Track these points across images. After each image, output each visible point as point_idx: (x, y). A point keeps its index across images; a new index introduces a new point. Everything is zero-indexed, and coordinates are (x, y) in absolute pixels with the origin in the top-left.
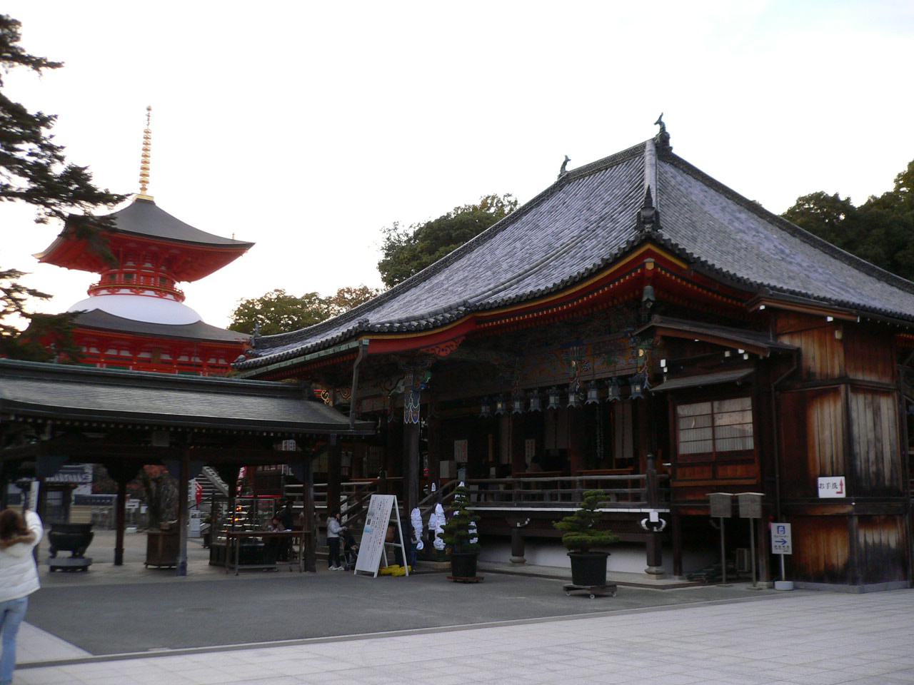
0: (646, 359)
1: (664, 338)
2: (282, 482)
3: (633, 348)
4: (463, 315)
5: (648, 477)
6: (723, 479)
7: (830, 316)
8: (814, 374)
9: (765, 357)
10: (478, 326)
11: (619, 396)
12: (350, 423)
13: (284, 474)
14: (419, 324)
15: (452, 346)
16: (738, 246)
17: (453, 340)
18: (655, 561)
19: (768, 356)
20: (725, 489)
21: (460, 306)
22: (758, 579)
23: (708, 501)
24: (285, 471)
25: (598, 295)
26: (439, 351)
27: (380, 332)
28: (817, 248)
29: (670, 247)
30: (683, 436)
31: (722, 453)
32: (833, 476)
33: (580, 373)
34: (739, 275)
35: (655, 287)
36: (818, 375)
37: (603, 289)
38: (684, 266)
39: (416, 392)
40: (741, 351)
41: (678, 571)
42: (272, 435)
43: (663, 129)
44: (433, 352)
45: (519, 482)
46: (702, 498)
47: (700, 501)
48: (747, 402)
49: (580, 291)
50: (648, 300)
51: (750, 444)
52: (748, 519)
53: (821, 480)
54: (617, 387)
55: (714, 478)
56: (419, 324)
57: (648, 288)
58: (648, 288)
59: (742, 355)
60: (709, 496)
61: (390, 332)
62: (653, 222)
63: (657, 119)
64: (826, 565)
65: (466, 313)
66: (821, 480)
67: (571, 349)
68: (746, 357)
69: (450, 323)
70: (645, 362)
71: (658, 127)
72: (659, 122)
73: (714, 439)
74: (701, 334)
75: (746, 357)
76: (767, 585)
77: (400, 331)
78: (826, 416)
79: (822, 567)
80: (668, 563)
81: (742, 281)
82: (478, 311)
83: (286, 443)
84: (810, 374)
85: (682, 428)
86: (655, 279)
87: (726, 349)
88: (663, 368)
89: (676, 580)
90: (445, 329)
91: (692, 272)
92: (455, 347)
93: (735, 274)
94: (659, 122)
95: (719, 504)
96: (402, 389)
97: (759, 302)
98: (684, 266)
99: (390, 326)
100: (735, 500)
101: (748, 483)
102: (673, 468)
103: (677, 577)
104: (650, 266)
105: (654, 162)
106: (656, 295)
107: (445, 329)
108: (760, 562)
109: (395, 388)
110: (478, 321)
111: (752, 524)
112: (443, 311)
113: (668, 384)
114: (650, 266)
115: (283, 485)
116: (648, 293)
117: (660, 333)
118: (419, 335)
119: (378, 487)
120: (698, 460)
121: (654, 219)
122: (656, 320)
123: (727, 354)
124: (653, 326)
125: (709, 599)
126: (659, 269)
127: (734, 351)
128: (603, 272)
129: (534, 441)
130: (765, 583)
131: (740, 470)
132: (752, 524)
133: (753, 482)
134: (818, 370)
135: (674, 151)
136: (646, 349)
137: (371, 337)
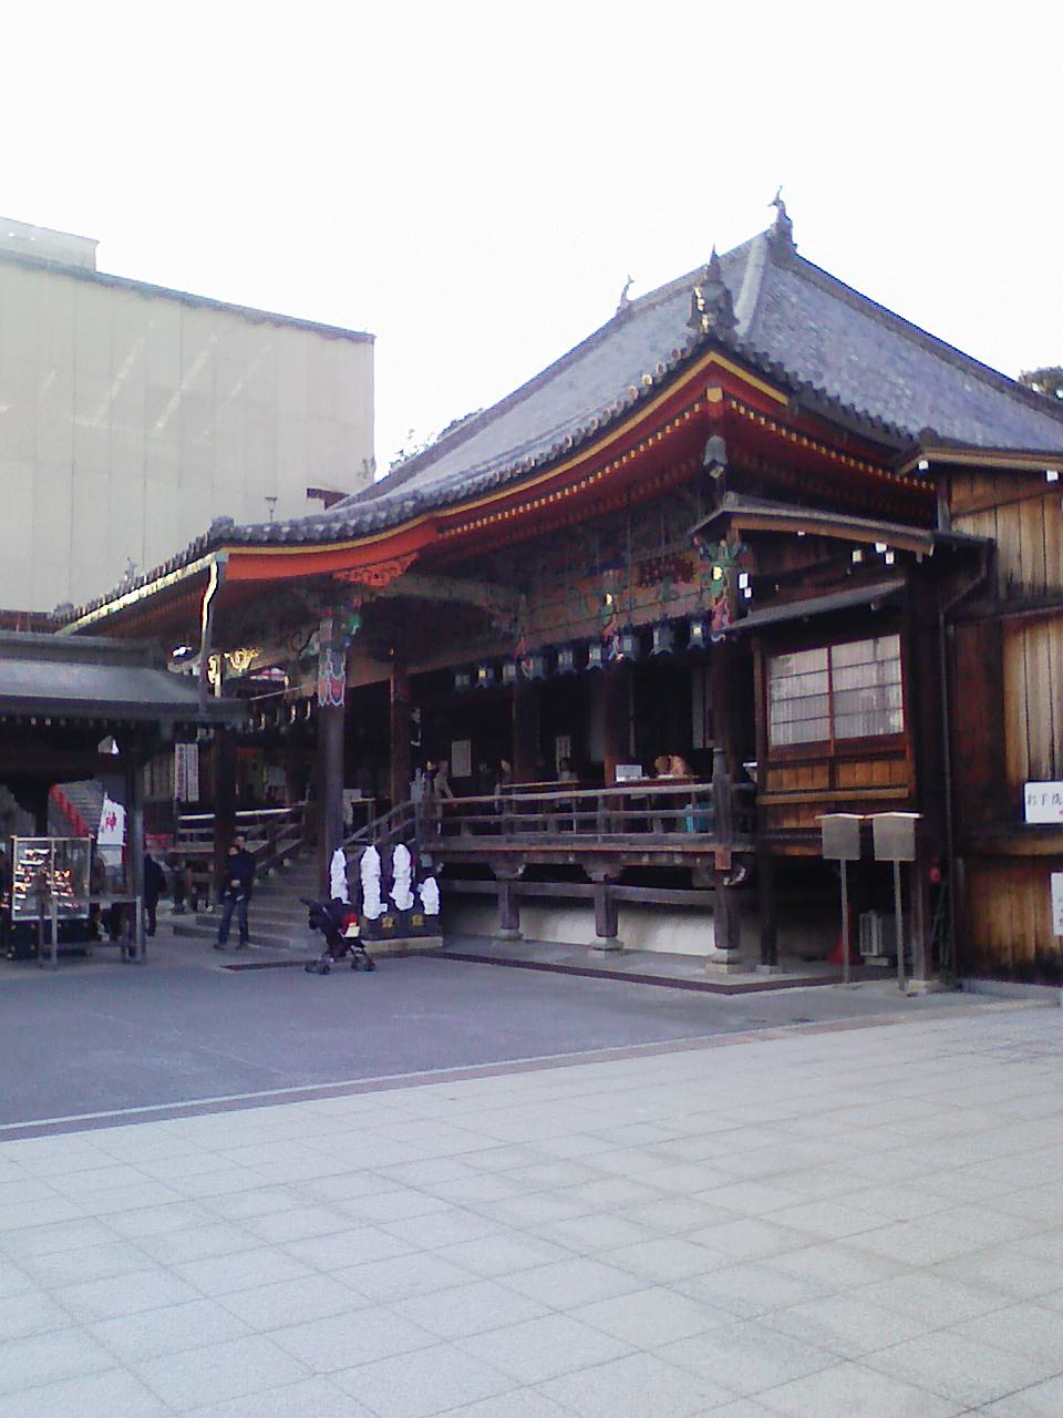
0: (725, 584)
1: (746, 536)
2: (174, 812)
3: (706, 567)
4: (411, 515)
5: (714, 787)
6: (844, 789)
7: (1052, 470)
8: (1020, 586)
9: (925, 556)
10: (440, 535)
11: (671, 644)
12: (199, 702)
13: (179, 799)
14: (328, 529)
15: (393, 569)
16: (899, 392)
17: (396, 559)
18: (728, 939)
19: (931, 553)
20: (850, 806)
21: (407, 500)
22: (909, 972)
23: (818, 830)
24: (179, 794)
25: (631, 462)
26: (370, 578)
27: (251, 542)
28: (1040, 410)
29: (753, 360)
30: (777, 714)
31: (845, 741)
32: (1053, 780)
33: (613, 614)
34: (888, 418)
35: (727, 438)
36: (1026, 588)
37: (636, 449)
38: (781, 398)
39: (338, 650)
40: (880, 548)
41: (770, 956)
42: (48, 722)
43: (782, 213)
44: (359, 579)
45: (510, 801)
46: (811, 825)
47: (805, 830)
48: (892, 645)
49: (598, 454)
50: (714, 464)
51: (897, 722)
52: (838, 862)
53: (1030, 789)
54: (668, 628)
55: (833, 787)
56: (328, 529)
57: (715, 441)
58: (715, 441)
59: (883, 555)
60: (821, 820)
61: (272, 541)
62: (720, 310)
63: (773, 199)
64: (1039, 950)
65: (417, 512)
66: (1031, 789)
67: (605, 574)
68: (890, 559)
69: (388, 528)
70: (725, 590)
71: (775, 210)
72: (777, 202)
73: (832, 716)
74: (805, 520)
75: (890, 559)
76: (926, 987)
77: (290, 541)
78: (1043, 669)
79: (1032, 953)
80: (751, 942)
81: (893, 431)
82: (436, 507)
83: (181, 749)
84: (1013, 587)
85: (776, 698)
86: (730, 425)
87: (854, 545)
88: (743, 590)
89: (764, 974)
90: (376, 538)
91: (797, 409)
92: (399, 573)
93: (879, 417)
94: (777, 202)
95: (837, 832)
96: (317, 647)
97: (917, 455)
98: (781, 398)
99: (271, 531)
100: (866, 830)
101: (291, 553)
102: (761, 770)
103: (767, 968)
104: (715, 395)
105: (762, 263)
106: (729, 452)
107: (376, 538)
108: (914, 943)
109: (306, 646)
110: (441, 525)
111: (897, 869)
112: (375, 509)
113: (756, 618)
114: (715, 395)
115: (178, 815)
116: (715, 450)
117: (737, 525)
118: (329, 548)
119: (304, 817)
120: (804, 756)
121: (722, 305)
122: (730, 502)
123: (857, 556)
124: (725, 513)
125: (801, 1019)
126: (734, 404)
127: (868, 549)
128: (633, 417)
129: (568, 739)
130: (923, 983)
131: (878, 772)
132: (897, 869)
133: (902, 793)
134: (1027, 577)
135: (799, 251)
136: (726, 566)
137: (235, 550)
